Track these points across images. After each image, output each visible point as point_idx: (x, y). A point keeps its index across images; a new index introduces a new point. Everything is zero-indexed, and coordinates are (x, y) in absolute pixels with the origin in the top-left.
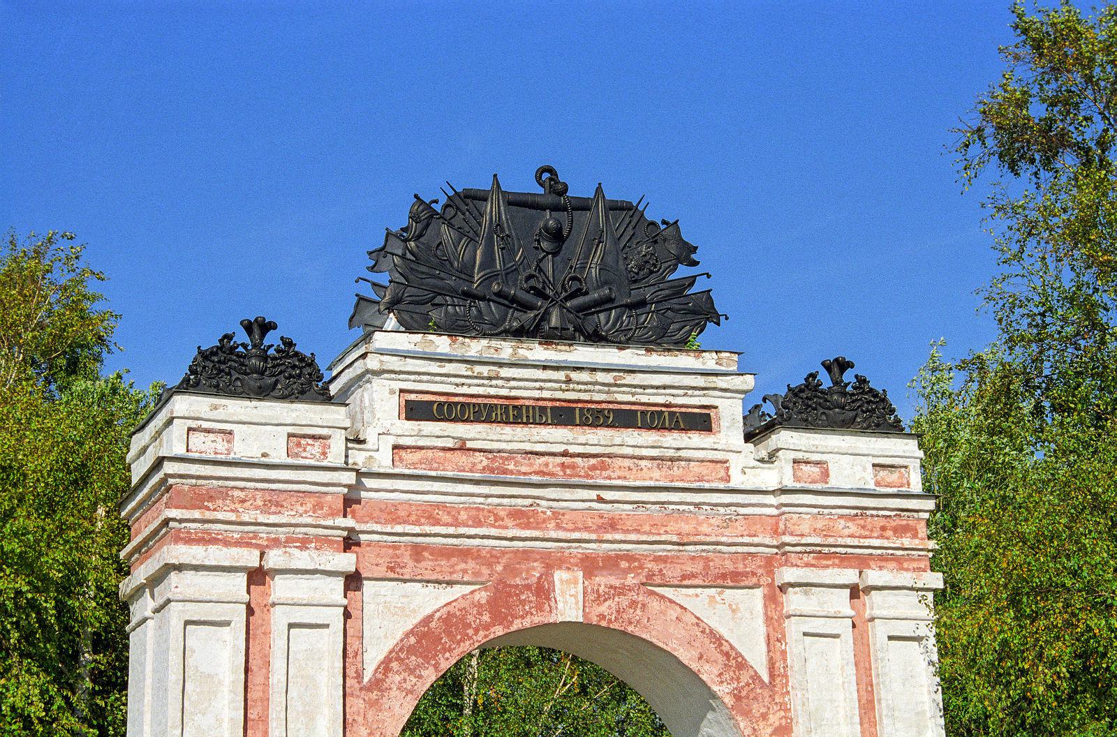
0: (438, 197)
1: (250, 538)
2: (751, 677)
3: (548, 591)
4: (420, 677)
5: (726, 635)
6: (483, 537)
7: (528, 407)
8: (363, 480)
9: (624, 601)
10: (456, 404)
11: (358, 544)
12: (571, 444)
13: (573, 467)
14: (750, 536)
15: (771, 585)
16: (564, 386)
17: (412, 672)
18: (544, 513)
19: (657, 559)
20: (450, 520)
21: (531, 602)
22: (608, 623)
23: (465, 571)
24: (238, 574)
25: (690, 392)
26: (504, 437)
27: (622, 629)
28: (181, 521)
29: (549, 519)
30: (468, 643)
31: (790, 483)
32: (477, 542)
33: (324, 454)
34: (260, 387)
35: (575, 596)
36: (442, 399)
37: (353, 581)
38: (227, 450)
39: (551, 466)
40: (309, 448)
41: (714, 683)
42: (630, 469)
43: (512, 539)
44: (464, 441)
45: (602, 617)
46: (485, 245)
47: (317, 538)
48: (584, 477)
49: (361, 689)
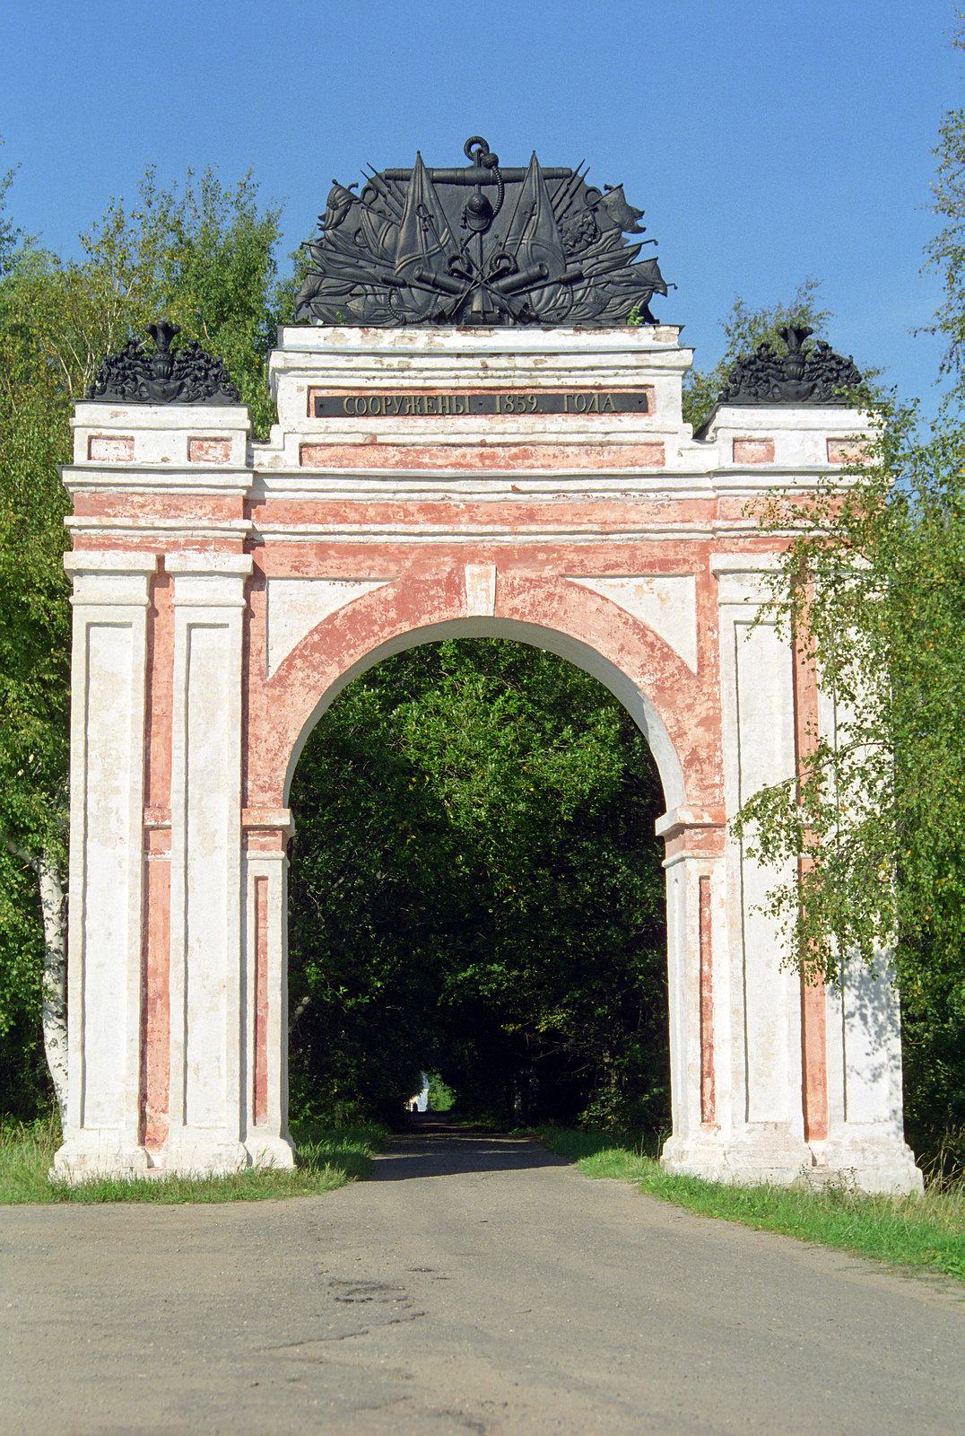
0: (356, 177)
1: (150, 543)
2: (677, 668)
3: (459, 586)
4: (324, 673)
5: (652, 624)
6: (390, 534)
7: (443, 397)
8: (266, 480)
9: (540, 594)
10: (367, 398)
11: (262, 544)
12: (489, 434)
13: (493, 457)
14: (683, 522)
15: (705, 573)
16: (481, 374)
17: (315, 668)
18: (457, 506)
19: (579, 550)
20: (357, 518)
21: (440, 597)
22: (521, 616)
23: (371, 568)
24: (138, 577)
25: (621, 372)
26: (416, 430)
27: (536, 622)
28: (80, 528)
29: (463, 512)
30: (373, 639)
31: (729, 465)
32: (384, 538)
33: (227, 456)
34: (797, 393)
35: (486, 590)
36: (355, 393)
37: (255, 580)
38: (130, 456)
39: (468, 457)
40: (211, 451)
41: (635, 674)
42: (555, 456)
43: (421, 534)
44: (374, 436)
45: (514, 610)
46: (408, 228)
47: (217, 540)
48: (504, 467)
49: (264, 686)
